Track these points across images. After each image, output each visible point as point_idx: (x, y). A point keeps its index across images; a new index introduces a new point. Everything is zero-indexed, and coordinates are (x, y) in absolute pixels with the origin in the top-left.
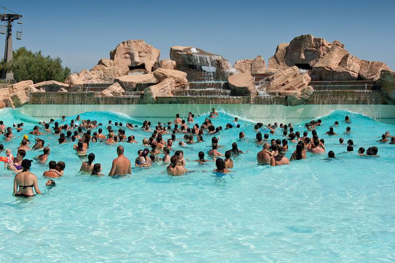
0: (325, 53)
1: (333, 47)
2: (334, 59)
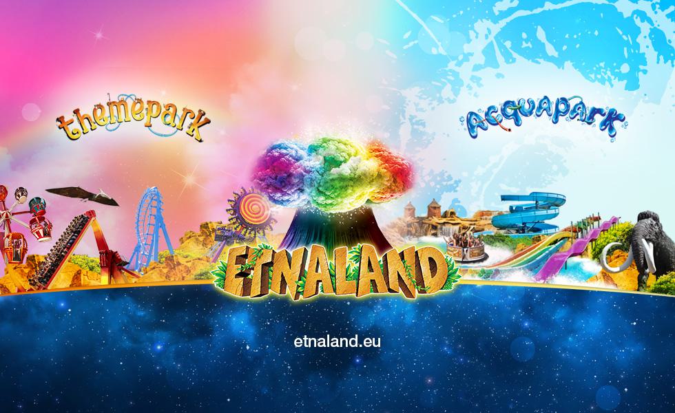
0: (184, 275)
1: (193, 264)
2: (60, 281)
